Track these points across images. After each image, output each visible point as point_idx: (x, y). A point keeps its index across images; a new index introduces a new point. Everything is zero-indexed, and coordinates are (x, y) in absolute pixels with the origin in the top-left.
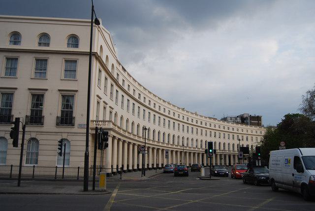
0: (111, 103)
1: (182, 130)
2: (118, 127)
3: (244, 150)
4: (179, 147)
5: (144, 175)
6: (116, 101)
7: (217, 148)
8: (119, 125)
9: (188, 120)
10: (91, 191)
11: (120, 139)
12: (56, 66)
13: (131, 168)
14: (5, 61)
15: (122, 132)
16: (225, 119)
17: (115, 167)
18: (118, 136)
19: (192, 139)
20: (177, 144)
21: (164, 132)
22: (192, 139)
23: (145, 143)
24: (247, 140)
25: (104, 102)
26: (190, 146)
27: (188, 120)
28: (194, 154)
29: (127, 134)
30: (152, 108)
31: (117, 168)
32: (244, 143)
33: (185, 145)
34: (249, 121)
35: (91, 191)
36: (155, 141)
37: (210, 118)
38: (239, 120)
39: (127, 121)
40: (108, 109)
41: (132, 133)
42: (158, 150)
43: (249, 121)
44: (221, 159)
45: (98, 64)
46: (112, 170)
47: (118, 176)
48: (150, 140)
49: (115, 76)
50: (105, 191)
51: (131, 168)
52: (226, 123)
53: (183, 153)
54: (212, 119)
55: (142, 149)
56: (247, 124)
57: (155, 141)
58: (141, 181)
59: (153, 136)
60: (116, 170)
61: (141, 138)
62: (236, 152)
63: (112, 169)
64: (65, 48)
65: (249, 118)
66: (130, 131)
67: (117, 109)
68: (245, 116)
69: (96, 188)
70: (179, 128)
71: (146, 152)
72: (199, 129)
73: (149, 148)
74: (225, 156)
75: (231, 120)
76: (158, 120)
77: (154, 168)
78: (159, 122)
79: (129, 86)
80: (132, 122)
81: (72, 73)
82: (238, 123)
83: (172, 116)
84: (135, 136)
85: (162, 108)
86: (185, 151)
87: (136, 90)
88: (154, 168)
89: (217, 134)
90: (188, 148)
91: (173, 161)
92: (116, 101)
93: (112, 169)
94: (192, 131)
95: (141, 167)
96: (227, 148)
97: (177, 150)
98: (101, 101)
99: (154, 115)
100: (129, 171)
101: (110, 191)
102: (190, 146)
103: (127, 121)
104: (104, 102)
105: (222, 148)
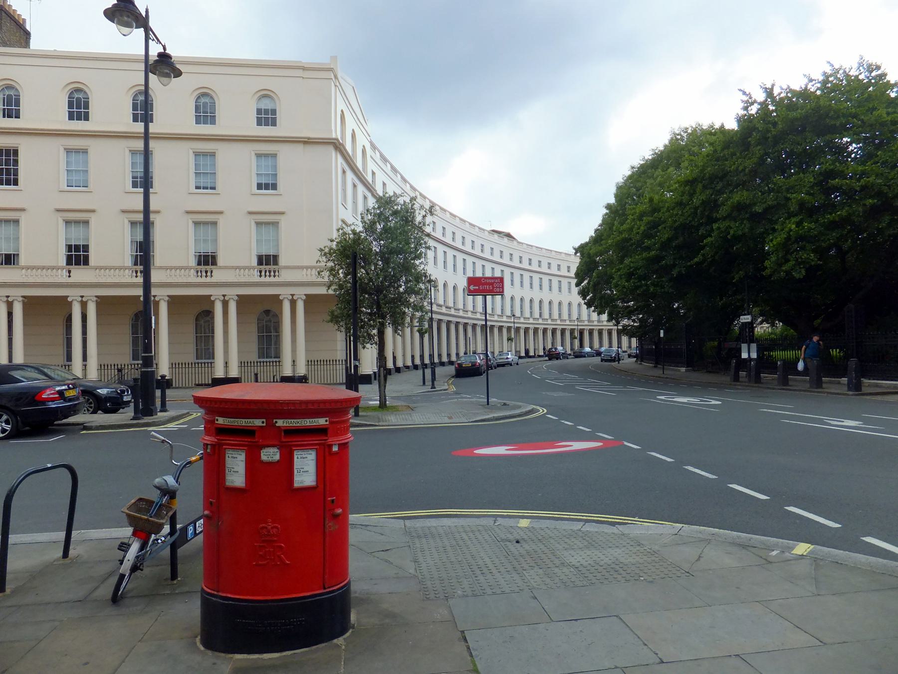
1: (567, 290)
4: (505, 319)
12: (237, 168)
13: (400, 364)
14: (63, 155)
23: (432, 312)
30: (460, 246)
33: (518, 314)
44: (573, 338)
45: (340, 160)
49: (369, 178)
61: (453, 310)
64: (190, 126)
72: (527, 275)
74: (581, 333)
77: (416, 367)
81: (81, 156)
83: (508, 262)
84: (441, 306)
86: (516, 325)
88: (416, 367)
89: (543, 281)
90: (522, 320)
95: (427, 361)
96: (565, 316)
97: (475, 322)
99: (445, 252)
100: (398, 370)
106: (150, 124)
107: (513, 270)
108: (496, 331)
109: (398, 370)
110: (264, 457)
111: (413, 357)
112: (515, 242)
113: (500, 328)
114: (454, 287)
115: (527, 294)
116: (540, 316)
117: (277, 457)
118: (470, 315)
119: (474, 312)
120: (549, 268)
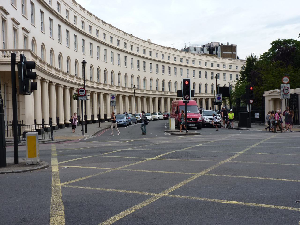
0: (24, 23)
1: (155, 70)
2: (48, 66)
3: (224, 91)
5: (86, 132)
6: (33, 20)
7: (197, 91)
8: (48, 62)
9: (144, 53)
10: (10, 165)
11: (59, 85)
13: (62, 122)
15: (53, 72)
16: (187, 50)
17: (40, 122)
18: (63, 83)
19: (126, 75)
20: (149, 89)
21: (106, 69)
22: (145, 79)
23: (85, 86)
24: (225, 78)
25: (24, 29)
26: (142, 87)
27: (150, 55)
28: (148, 99)
29: (61, 75)
31: (43, 124)
32: (222, 83)
34: (219, 52)
35: (10, 165)
36: (107, 85)
37: (169, 48)
38: (206, 50)
39: (68, 59)
40: (21, 33)
41: (98, 83)
42: (99, 94)
43: (219, 52)
46: (36, 128)
47: (48, 135)
48: (93, 82)
50: (38, 164)
51: (62, 122)
52: (190, 55)
53: (135, 98)
54: (172, 50)
55: (79, 95)
56: (216, 55)
57: (107, 85)
58: (83, 141)
59: (163, 86)
60: (41, 126)
62: (210, 95)
63: (36, 125)
65: (219, 48)
66: (65, 71)
67: (35, 32)
68: (214, 46)
69: (20, 160)
70: (157, 70)
71: (89, 97)
72: (154, 64)
73: (92, 93)
75: (195, 50)
76: (81, 46)
77: (95, 122)
78: (98, 53)
79: (67, 11)
80: (75, 60)
82: (205, 54)
84: (72, 76)
85: (101, 33)
86: (136, 95)
87: (71, 12)
88: (95, 122)
89: (171, 68)
91: (124, 111)
92: (33, 20)
93: (36, 125)
94: (163, 71)
97: (93, 90)
98: (19, 28)
101: (46, 164)
102: (123, 85)
103: (68, 59)
104: (24, 29)
105: (203, 91)
106: (178, 50)
107: (145, 60)
108: (121, 99)
109: (60, 127)
110: (258, 117)
111: (51, 119)
112: (178, 52)
113: (124, 97)
114: (75, 62)
115: (167, 78)
116: (157, 90)
117: (256, 117)
118: (102, 87)
119: (112, 86)
120: (175, 60)
